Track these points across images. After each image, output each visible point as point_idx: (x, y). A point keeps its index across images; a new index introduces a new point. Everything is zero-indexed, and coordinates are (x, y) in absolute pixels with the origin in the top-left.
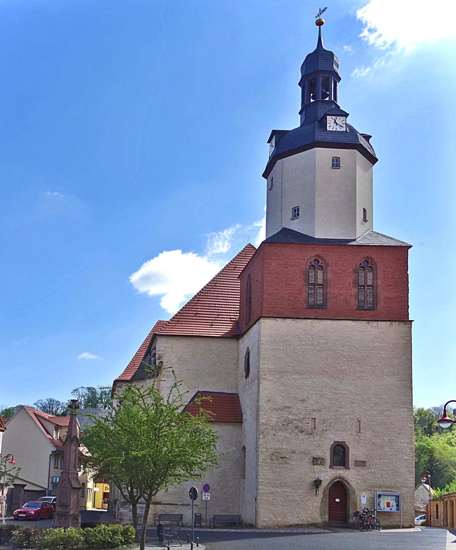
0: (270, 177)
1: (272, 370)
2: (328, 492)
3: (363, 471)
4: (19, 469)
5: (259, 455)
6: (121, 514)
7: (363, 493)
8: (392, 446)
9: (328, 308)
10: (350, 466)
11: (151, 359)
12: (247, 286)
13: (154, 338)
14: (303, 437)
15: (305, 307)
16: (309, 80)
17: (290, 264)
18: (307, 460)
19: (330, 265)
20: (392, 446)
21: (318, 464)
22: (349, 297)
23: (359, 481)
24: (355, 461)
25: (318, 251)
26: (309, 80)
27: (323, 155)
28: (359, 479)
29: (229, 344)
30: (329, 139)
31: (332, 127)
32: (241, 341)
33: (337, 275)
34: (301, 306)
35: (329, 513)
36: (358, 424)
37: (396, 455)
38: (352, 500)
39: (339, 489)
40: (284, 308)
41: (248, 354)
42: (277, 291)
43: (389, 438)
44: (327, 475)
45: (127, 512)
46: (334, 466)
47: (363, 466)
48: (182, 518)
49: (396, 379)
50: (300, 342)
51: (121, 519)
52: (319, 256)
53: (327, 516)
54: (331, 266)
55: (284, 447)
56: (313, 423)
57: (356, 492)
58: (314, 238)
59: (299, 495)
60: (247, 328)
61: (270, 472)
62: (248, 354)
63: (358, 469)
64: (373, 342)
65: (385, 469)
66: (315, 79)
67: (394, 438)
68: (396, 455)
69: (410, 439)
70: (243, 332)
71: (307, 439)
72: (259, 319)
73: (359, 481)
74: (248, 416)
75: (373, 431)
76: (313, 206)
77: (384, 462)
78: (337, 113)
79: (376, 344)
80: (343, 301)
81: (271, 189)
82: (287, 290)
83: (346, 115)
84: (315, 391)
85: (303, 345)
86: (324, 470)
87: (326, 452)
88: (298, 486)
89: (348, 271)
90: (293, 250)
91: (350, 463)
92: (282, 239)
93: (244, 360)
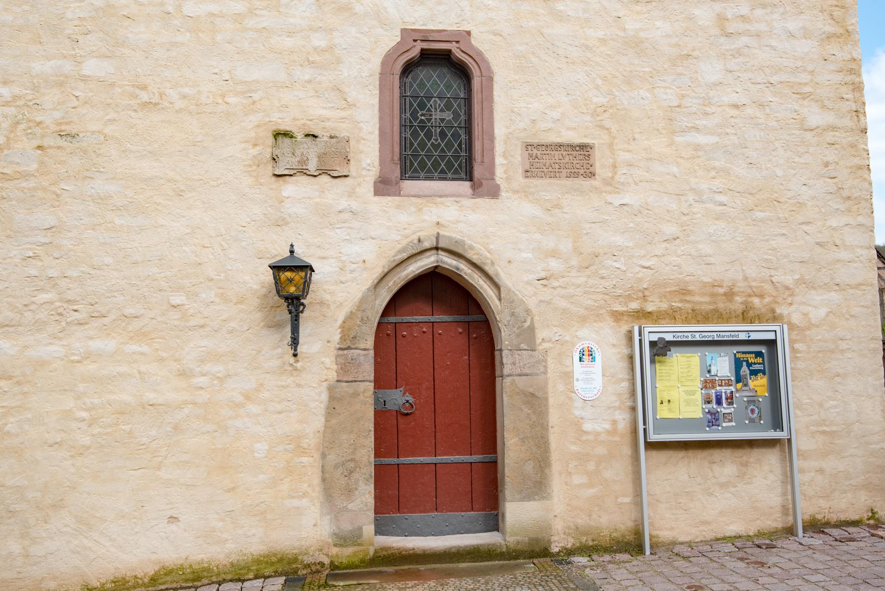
3: (576, 203)
4: (25, 305)
7: (584, 332)
10: (499, 172)
18: (239, 147)
20: (738, 53)
21: (304, 172)
23: (554, 265)
28: (554, 254)
38: (521, 382)
39: (441, 319)
44: (365, 236)
47: (576, 175)
55: (91, 67)
59: (183, 374)
63: (550, 189)
65: (704, 186)
69: (837, 13)
73: (554, 265)
77: (697, 147)
86: (344, 204)
87: (353, 94)
91: (499, 160)
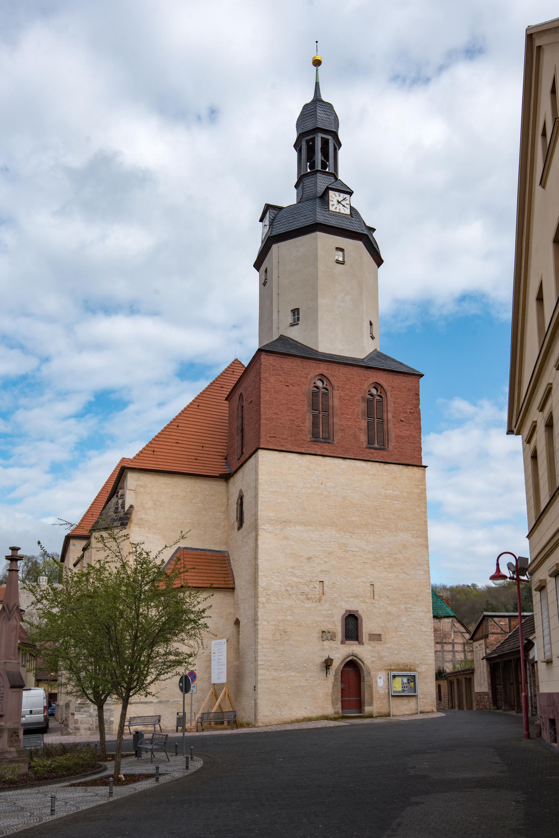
0: (263, 268)
1: (273, 518)
2: (340, 674)
3: (378, 646)
5: (257, 629)
6: (76, 722)
7: (380, 673)
8: (409, 615)
9: (335, 442)
11: (117, 502)
12: (238, 410)
13: (123, 471)
14: (310, 605)
15: (309, 440)
16: (306, 141)
17: (291, 382)
19: (336, 388)
20: (409, 615)
21: (328, 640)
22: (357, 431)
23: (374, 659)
24: (369, 634)
25: (323, 369)
26: (306, 141)
27: (324, 242)
28: (374, 657)
29: (218, 486)
30: (333, 222)
31: (334, 207)
32: (232, 480)
33: (344, 402)
34: (304, 437)
35: (342, 701)
36: (372, 589)
37: (413, 626)
38: (368, 683)
40: (286, 439)
41: (241, 498)
42: (277, 416)
43: (405, 605)
44: (340, 652)
45: (86, 718)
46: (346, 642)
48: (159, 720)
49: (411, 535)
50: (304, 484)
51: (77, 729)
52: (324, 376)
53: (339, 705)
54: (338, 390)
55: (289, 618)
56: (322, 588)
57: (372, 673)
58: (318, 351)
60: (239, 465)
61: (273, 651)
62: (241, 498)
63: (373, 643)
64: (385, 490)
66: (313, 140)
67: (410, 606)
68: (413, 626)
70: (233, 470)
71: (315, 607)
72: (256, 451)
73: (374, 659)
74: (241, 581)
75: (388, 597)
76: (314, 310)
77: (401, 635)
78: (341, 189)
79: (388, 492)
80: (351, 435)
81: (265, 284)
82: (288, 415)
83: (350, 193)
84: (322, 547)
85: (308, 488)
86: (335, 646)
87: (336, 623)
88: (305, 668)
89: (356, 398)
90: (294, 365)
91: (364, 637)
92: (278, 350)
93: (235, 506)
